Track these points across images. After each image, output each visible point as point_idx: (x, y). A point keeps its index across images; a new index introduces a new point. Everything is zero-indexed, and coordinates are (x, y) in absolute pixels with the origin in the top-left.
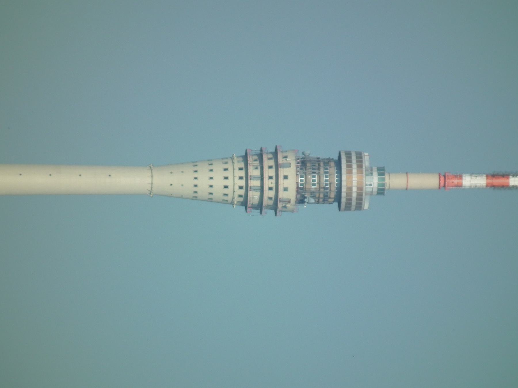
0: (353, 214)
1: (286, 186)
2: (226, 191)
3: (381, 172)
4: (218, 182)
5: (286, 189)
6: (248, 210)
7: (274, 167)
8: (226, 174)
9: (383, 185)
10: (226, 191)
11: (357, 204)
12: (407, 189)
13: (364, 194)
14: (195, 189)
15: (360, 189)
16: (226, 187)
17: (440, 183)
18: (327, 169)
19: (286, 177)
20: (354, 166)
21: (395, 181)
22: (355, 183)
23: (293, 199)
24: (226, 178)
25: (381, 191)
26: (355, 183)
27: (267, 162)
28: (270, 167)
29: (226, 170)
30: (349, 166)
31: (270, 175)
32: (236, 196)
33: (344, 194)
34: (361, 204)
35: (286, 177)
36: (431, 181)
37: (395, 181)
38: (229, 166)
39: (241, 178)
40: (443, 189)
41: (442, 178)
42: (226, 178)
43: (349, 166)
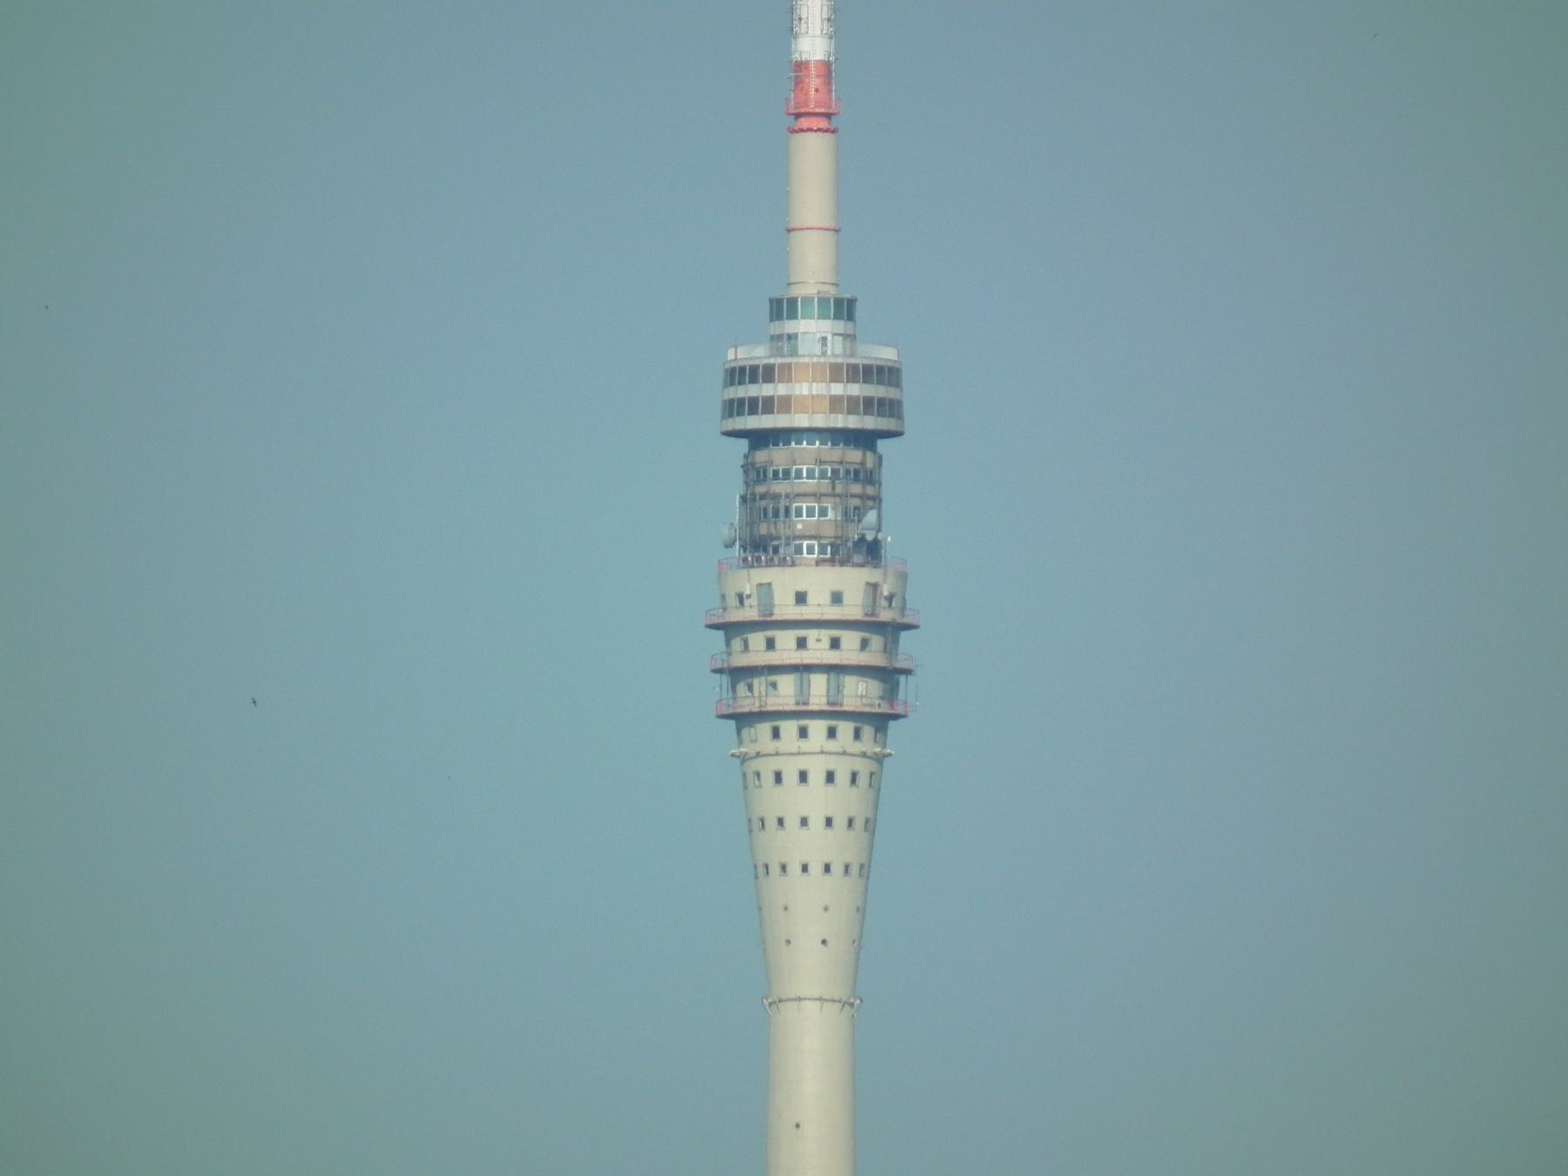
0: (911, 394)
1: (827, 599)
2: (842, 778)
3: (783, 308)
4: (816, 800)
5: (837, 598)
6: (899, 710)
7: (770, 633)
8: (791, 777)
9: (823, 301)
10: (842, 778)
11: (880, 382)
12: (837, 231)
13: (852, 361)
14: (837, 869)
15: (836, 373)
16: (830, 777)
17: (819, 130)
18: (776, 473)
19: (801, 598)
20: (766, 390)
21: (812, 267)
22: (818, 388)
23: (868, 574)
24: (803, 777)
25: (844, 309)
26: (818, 388)
27: (757, 654)
28: (771, 644)
29: (778, 777)
30: (768, 405)
31: (793, 645)
32: (857, 747)
33: (853, 422)
34: (880, 369)
35: (801, 598)
36: (812, 156)
37: (812, 267)
38: (767, 767)
39: (803, 733)
40: (835, 122)
41: (804, 123)
42: (803, 777)
43: (768, 405)
